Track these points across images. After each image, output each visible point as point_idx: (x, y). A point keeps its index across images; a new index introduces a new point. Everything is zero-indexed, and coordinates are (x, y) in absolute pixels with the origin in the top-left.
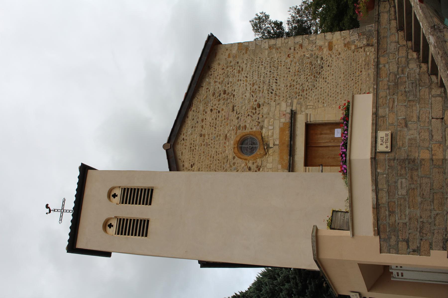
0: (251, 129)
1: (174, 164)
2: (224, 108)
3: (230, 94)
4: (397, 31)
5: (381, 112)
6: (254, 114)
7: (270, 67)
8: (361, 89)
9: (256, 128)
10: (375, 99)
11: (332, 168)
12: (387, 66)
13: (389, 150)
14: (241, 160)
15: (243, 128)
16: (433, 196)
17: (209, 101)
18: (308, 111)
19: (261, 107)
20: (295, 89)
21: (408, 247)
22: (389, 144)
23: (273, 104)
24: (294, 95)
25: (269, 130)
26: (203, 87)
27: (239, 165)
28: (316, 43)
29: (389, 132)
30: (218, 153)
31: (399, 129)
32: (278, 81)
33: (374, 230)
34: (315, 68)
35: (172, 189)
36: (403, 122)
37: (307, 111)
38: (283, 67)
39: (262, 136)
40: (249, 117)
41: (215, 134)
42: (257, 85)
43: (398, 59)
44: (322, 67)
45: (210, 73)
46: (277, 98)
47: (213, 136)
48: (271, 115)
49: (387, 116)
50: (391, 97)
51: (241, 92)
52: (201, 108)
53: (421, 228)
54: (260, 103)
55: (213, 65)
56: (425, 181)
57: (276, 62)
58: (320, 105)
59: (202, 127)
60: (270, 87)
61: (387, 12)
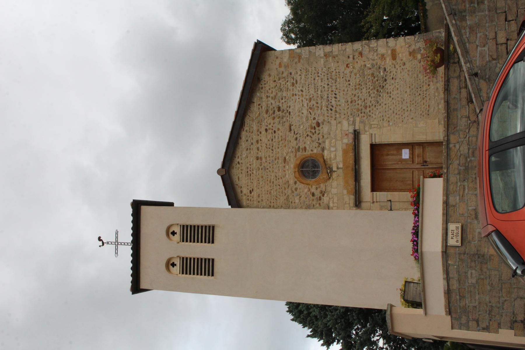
0: (312, 151)
1: (234, 200)
2: (280, 128)
3: (285, 111)
4: (468, 103)
5: (452, 200)
6: (313, 134)
7: (328, 79)
8: (429, 106)
9: (317, 150)
10: (446, 185)
11: (401, 193)
12: (457, 146)
13: (459, 244)
14: (303, 185)
15: (302, 150)
16: (502, 286)
17: (263, 119)
18: (374, 131)
19: (321, 126)
20: (357, 105)
21: (478, 325)
22: (459, 238)
23: (333, 122)
24: (356, 112)
25: (331, 152)
26: (254, 103)
27: (301, 191)
28: (377, 50)
29: (459, 225)
30: (278, 177)
31: (469, 221)
32: (337, 96)
33: (446, 311)
34: (377, 80)
35: (235, 228)
36: (473, 213)
37: (371, 131)
38: (342, 79)
39: (324, 159)
40: (309, 138)
41: (272, 157)
42: (314, 100)
43: (469, 138)
44: (386, 80)
45: (261, 86)
46: (338, 116)
47: (271, 158)
48: (332, 135)
49: (457, 206)
50: (462, 183)
51: (297, 108)
52: (255, 128)
53: (490, 311)
54: (320, 122)
55: (263, 76)
56: (493, 273)
57: (334, 73)
58: (385, 124)
59: (258, 149)
60: (329, 102)
61: (457, 77)
